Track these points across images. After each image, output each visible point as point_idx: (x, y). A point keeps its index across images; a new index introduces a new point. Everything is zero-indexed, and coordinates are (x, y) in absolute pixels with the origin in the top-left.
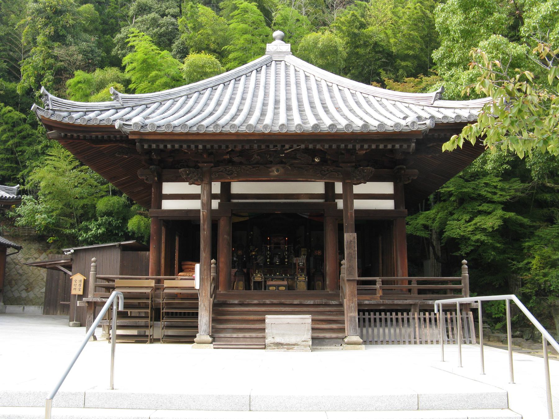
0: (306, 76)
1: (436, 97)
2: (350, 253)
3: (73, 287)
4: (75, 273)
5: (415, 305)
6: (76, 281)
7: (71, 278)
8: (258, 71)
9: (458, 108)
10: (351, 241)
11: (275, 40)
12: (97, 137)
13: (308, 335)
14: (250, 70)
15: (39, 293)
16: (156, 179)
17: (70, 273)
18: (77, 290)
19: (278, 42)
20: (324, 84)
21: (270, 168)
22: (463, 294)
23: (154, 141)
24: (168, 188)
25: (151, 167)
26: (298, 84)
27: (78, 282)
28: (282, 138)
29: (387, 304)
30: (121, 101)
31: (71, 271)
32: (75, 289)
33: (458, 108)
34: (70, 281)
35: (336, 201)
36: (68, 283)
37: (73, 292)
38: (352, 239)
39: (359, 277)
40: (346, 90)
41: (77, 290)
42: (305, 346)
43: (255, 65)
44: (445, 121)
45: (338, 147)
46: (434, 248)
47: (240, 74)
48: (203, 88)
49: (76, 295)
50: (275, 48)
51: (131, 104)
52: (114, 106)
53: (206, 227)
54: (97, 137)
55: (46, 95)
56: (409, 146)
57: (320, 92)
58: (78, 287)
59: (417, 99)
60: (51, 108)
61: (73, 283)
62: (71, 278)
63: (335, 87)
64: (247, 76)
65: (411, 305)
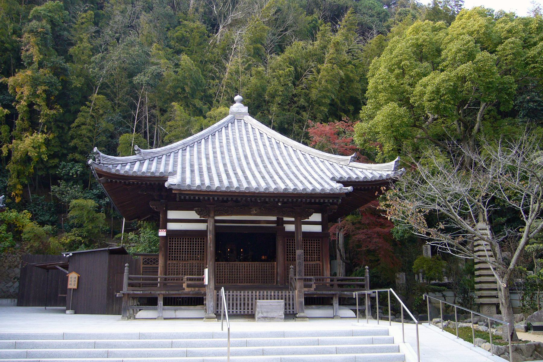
0: (261, 134)
1: (351, 159)
2: (300, 262)
3: (69, 283)
4: (70, 272)
5: (335, 294)
6: (71, 277)
7: (67, 275)
8: (227, 127)
9: (365, 169)
10: (300, 255)
11: (235, 103)
12: (133, 183)
13: (282, 313)
14: (221, 127)
15: (5, 287)
16: (165, 208)
17: (68, 272)
18: (73, 285)
19: (237, 105)
20: (273, 141)
21: (251, 209)
22: (365, 288)
23: (188, 194)
24: (172, 214)
25: (162, 201)
26: (255, 139)
27: (73, 278)
28: (266, 195)
29: (319, 294)
30: (142, 155)
31: (67, 270)
32: (71, 284)
33: (365, 169)
34: (67, 278)
35: (284, 225)
36: (65, 280)
37: (69, 287)
38: (503, 339)
39: (387, 291)
40: (289, 147)
41: (73, 285)
42: (281, 319)
43: (224, 123)
44: (357, 180)
45: (297, 200)
46: (340, 251)
47: (215, 130)
48: (192, 142)
49: (71, 289)
50: (237, 109)
51: (149, 157)
52: (139, 159)
53: (211, 245)
54: (133, 183)
55: (98, 153)
56: (338, 201)
57: (272, 148)
58: (73, 283)
59: (338, 159)
60: (102, 162)
61: (69, 279)
62: (67, 275)
63: (281, 144)
64: (220, 131)
65: (333, 294)
